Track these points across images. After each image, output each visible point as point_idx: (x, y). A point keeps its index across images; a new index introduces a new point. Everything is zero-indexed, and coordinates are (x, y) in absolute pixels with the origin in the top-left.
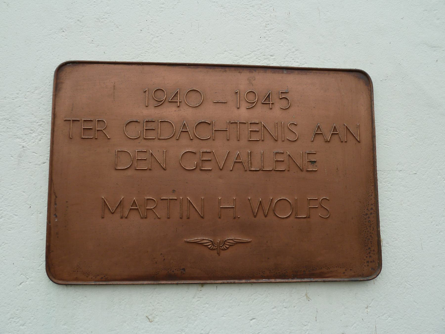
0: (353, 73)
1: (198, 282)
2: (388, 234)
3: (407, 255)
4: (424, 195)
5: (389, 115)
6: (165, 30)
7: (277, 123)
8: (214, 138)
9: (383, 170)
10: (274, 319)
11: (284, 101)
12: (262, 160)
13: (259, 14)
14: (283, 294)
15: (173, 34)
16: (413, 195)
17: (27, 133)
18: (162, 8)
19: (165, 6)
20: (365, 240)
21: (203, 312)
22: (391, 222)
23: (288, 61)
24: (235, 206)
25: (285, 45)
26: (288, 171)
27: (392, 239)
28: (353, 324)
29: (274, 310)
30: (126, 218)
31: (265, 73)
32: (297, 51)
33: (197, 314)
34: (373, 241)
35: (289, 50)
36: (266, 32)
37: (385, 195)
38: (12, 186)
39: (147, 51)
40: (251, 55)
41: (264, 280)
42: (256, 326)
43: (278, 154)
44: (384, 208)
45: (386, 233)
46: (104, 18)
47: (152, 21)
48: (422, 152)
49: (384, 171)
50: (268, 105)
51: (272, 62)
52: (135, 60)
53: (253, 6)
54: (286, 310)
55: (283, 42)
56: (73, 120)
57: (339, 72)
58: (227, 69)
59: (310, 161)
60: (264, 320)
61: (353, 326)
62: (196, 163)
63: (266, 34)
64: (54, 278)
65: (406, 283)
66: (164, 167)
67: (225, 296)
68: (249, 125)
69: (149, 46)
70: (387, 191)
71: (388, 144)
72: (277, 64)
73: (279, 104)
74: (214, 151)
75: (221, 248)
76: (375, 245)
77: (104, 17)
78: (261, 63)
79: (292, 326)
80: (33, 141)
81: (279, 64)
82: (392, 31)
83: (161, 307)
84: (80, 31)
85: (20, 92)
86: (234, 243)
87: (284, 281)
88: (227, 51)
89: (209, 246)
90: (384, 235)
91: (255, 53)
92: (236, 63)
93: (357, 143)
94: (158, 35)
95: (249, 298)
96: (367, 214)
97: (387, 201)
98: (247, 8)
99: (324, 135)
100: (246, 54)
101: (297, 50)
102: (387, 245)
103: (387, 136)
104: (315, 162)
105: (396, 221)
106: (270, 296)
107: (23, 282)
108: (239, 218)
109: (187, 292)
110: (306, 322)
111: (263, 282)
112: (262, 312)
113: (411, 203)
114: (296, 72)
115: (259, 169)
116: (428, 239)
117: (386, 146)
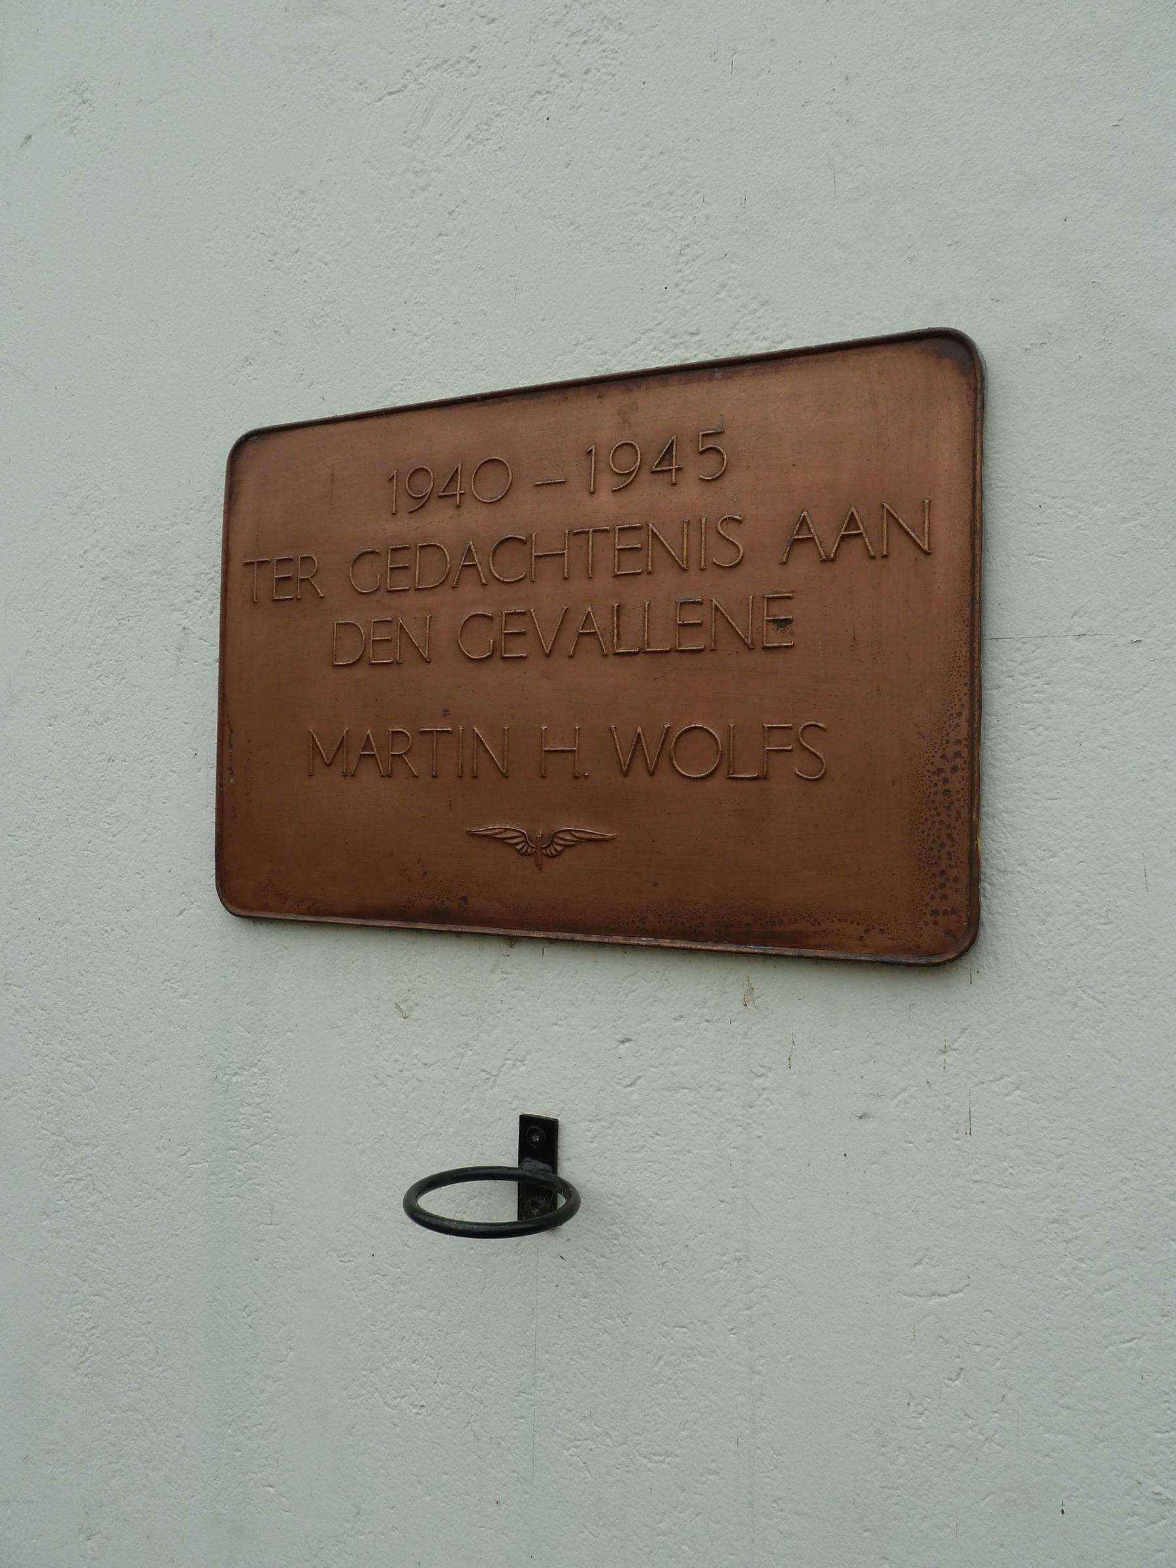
0: (923, 344)
1: (500, 931)
2: (1026, 835)
3: (1088, 903)
4: (1165, 714)
5: (1052, 459)
6: (443, 319)
7: (688, 523)
8: (535, 575)
9: (1021, 634)
10: (679, 1048)
11: (711, 458)
12: (646, 624)
13: (665, 220)
14: (703, 983)
15: (460, 323)
16: (1125, 713)
17: (191, 598)
18: (437, 262)
19: (444, 256)
20: (931, 849)
21: (512, 1009)
22: (1037, 797)
23: (737, 342)
24: (579, 748)
25: (730, 296)
26: (713, 650)
27: (1040, 852)
28: (900, 1093)
29: (678, 1023)
30: (353, 776)
31: (665, 386)
32: (764, 305)
33: (499, 1011)
34: (955, 852)
35: (742, 309)
36: (680, 271)
37: (1022, 715)
38: (168, 712)
39: (406, 377)
40: (639, 342)
41: (645, 941)
42: (634, 1058)
43: (687, 607)
44: (1017, 754)
45: (1021, 832)
46: (323, 316)
47: (416, 301)
48: (1166, 569)
49: (1024, 640)
50: (667, 475)
51: (695, 353)
52: (381, 405)
53: (649, 202)
54: (710, 1027)
55: (725, 289)
56: (258, 562)
57: (876, 349)
58: (570, 393)
59: (774, 621)
60: (652, 1047)
61: (899, 1098)
62: (492, 641)
63: (680, 274)
64: (230, 902)
65: (1080, 992)
66: (426, 656)
67: (563, 974)
68: (617, 535)
69: (408, 366)
70: (1030, 702)
71: (1042, 552)
72: (708, 354)
73: (696, 468)
74: (532, 610)
75: (544, 851)
76: (961, 862)
77: (323, 313)
78: (665, 360)
79: (724, 1072)
80: (200, 614)
81: (712, 354)
82: (1075, 177)
83: (424, 986)
84: (279, 356)
85: (179, 512)
86: (573, 841)
87: (693, 946)
88: (582, 343)
89: (519, 847)
90: (1013, 837)
91: (651, 334)
92: (601, 372)
93: (921, 556)
94: (427, 334)
95: (619, 985)
96: (940, 771)
97: (1030, 732)
98: (634, 214)
99: (817, 542)
100: (626, 343)
101: (764, 304)
102: (1019, 869)
103: (1038, 528)
104: (789, 621)
105: (1058, 796)
106: (668, 986)
107: (184, 910)
108: (587, 777)
109: (479, 956)
110: (762, 1066)
111: (640, 943)
112: (647, 1024)
113: (1116, 738)
114: (748, 369)
115: (637, 650)
116: (1171, 858)
117: (1035, 558)
